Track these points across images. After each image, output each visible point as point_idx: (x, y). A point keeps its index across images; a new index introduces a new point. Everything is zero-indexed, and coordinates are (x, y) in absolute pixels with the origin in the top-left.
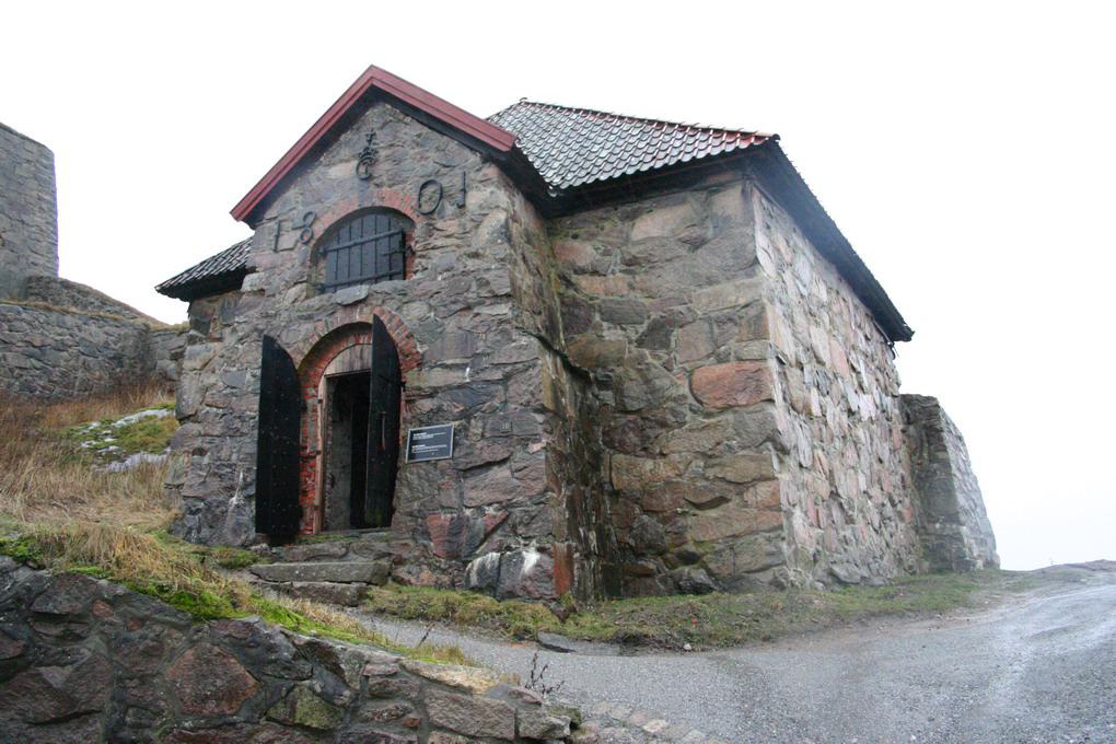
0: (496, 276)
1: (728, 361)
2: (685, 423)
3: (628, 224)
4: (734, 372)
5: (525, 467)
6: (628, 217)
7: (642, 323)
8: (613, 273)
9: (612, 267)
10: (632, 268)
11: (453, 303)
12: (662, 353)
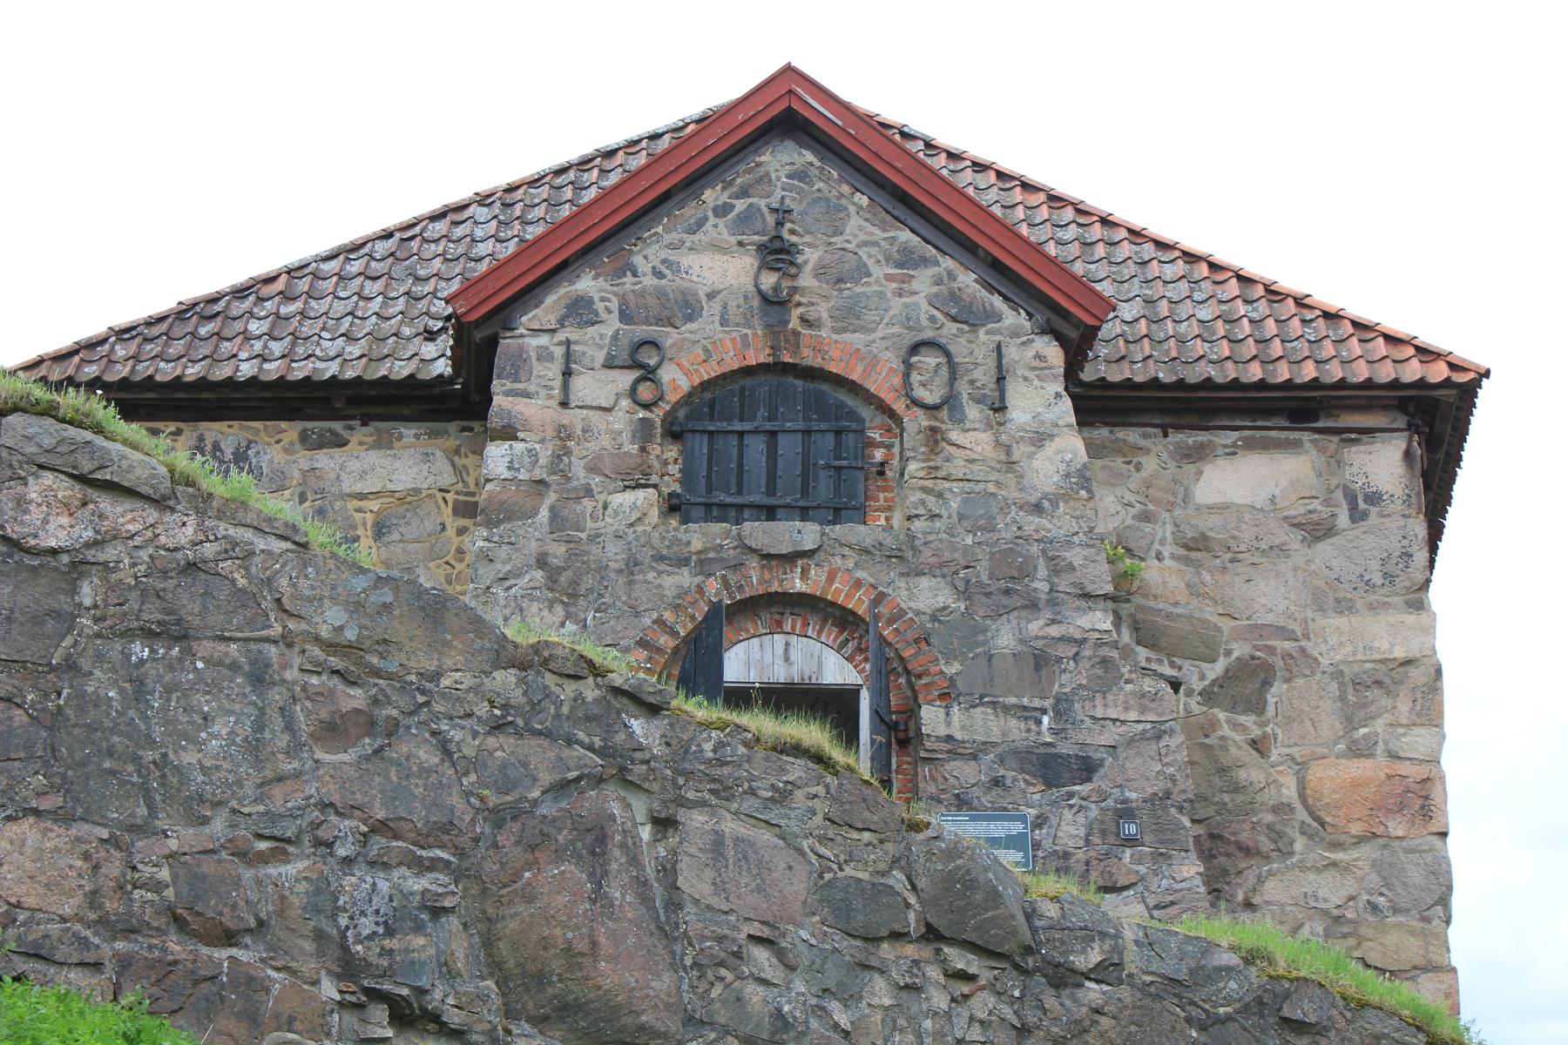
0: (1086, 558)
1: (1372, 756)
2: (1292, 853)
3: (1190, 468)
4: (1382, 776)
5: (1173, 903)
6: (1187, 456)
7: (1213, 661)
8: (1159, 557)
9: (1156, 546)
10: (1194, 555)
11: (1007, 592)
12: (1249, 720)
